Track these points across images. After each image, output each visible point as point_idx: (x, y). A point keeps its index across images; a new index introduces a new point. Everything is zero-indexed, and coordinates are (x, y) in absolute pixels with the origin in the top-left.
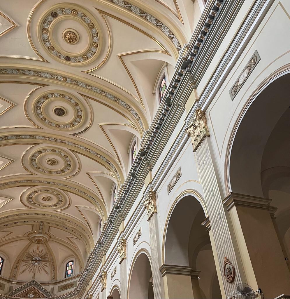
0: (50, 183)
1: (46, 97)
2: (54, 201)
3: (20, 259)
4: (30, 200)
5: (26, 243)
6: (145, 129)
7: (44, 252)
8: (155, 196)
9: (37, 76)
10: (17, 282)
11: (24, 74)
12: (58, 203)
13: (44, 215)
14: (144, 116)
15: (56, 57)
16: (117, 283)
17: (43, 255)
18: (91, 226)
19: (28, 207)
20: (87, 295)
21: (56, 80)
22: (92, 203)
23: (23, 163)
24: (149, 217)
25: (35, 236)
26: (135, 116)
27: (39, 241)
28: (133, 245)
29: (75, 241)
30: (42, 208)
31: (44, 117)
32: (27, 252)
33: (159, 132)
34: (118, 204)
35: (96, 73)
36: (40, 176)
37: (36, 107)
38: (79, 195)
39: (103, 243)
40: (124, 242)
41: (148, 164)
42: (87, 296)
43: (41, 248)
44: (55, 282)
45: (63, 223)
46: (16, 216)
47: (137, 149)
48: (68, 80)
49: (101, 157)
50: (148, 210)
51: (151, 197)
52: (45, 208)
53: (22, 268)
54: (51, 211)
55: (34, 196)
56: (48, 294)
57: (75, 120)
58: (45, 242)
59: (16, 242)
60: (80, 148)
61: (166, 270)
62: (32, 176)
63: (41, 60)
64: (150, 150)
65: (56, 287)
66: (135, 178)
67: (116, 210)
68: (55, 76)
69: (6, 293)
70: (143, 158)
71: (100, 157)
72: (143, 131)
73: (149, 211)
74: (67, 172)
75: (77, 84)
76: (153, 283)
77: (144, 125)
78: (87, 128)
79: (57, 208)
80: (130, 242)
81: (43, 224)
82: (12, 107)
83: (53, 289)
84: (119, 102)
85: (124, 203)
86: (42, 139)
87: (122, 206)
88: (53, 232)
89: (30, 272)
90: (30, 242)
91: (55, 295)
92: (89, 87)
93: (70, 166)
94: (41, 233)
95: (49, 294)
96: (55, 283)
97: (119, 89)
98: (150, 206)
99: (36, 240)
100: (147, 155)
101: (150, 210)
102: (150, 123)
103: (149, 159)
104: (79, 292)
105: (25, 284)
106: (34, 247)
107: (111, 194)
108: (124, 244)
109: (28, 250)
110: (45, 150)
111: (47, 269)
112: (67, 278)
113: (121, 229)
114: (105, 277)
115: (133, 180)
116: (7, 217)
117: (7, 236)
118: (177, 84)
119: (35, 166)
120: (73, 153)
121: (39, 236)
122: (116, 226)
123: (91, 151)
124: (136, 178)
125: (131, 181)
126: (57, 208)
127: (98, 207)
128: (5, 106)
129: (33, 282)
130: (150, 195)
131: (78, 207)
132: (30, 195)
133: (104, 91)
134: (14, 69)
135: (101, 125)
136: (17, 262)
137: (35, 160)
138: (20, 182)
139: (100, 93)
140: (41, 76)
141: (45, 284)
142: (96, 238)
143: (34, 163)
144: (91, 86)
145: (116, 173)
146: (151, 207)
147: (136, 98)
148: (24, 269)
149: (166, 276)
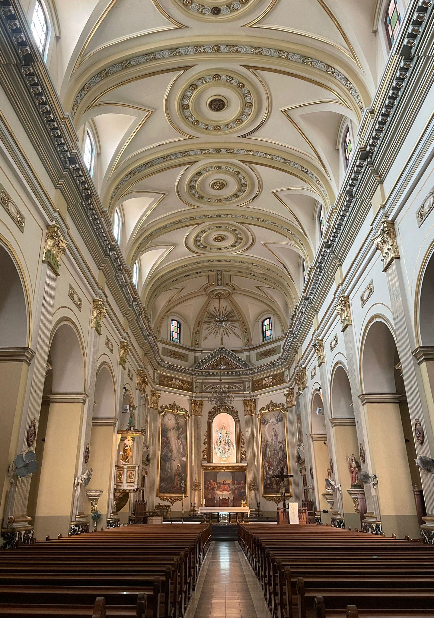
0: (221, 215)
1: (193, 86)
2: (231, 240)
3: (200, 321)
4: (199, 243)
5: (202, 300)
6: (363, 105)
7: (229, 308)
8: (394, 229)
9: (174, 56)
10: (202, 351)
11: (155, 59)
12: (236, 242)
13: (220, 261)
14: (360, 80)
15: (196, 14)
16: (340, 358)
17: (228, 313)
18: (290, 271)
19: (197, 253)
20: (298, 366)
21: (204, 54)
22: (286, 236)
23: (179, 195)
24: (385, 266)
25: (214, 290)
26: (344, 83)
27: (219, 296)
28: (361, 307)
29: (270, 292)
30: (215, 252)
31: (196, 119)
32: (207, 310)
33: (393, 114)
34: (328, 241)
35: (265, 22)
36: (206, 208)
37: (181, 106)
38: (264, 227)
39: (312, 297)
40: (346, 299)
41: (376, 172)
42: (298, 368)
43: (224, 303)
44: (251, 347)
45: (248, 269)
46: (185, 268)
47: (352, 140)
48: (222, 48)
49: (292, 163)
50: (382, 252)
51: (386, 231)
52: (220, 251)
53: (204, 333)
54: (228, 254)
55: (202, 238)
56: (243, 364)
57: (242, 113)
58: (228, 296)
59: (192, 299)
60: (257, 155)
61: (424, 355)
62: (194, 210)
63: (176, 27)
64: (378, 146)
65: (253, 354)
66: (354, 197)
67: (326, 250)
68: (201, 48)
69: (191, 365)
70: (365, 163)
71: (290, 165)
72: (361, 107)
73: (384, 255)
74: (242, 196)
75: (237, 52)
76: (402, 371)
77: (361, 97)
78: (264, 120)
79: (236, 250)
80: (355, 301)
81: (221, 273)
82: (149, 115)
83: (249, 357)
84: (311, 63)
85: (338, 238)
86: (199, 153)
87: (335, 244)
88: (236, 281)
89: (216, 336)
90: (208, 298)
91: (253, 365)
92: (257, 50)
93: (245, 186)
94: (221, 284)
95: (245, 364)
96: (251, 349)
97: (310, 40)
98: (386, 248)
99: (216, 294)
100: (372, 156)
101: (386, 253)
102: (373, 92)
103: (376, 164)
104: (285, 362)
105: (212, 352)
106: (215, 304)
107: (315, 220)
108: (346, 303)
109: (208, 309)
110: (205, 169)
111: (237, 331)
112: (265, 342)
113: (338, 278)
114: (322, 346)
115: (350, 201)
116: (174, 270)
117: (178, 293)
118: (421, 15)
119: (197, 196)
120: (246, 165)
121: (218, 289)
122: (329, 274)
123: (274, 158)
124: (356, 198)
125: (347, 204)
126: (236, 250)
127: (296, 241)
128: (139, 117)
129: (222, 349)
130: (384, 227)
131: (267, 245)
132: (197, 237)
133: (283, 51)
134: (139, 56)
135: (284, 111)
136: (197, 325)
137: (194, 187)
138: (180, 221)
139: (276, 55)
140: (180, 55)
141: (237, 351)
142: (299, 289)
143: (194, 191)
144: (260, 48)
145: (319, 186)
146: (388, 249)
147: (342, 49)
148: (207, 333)
149: (424, 364)
